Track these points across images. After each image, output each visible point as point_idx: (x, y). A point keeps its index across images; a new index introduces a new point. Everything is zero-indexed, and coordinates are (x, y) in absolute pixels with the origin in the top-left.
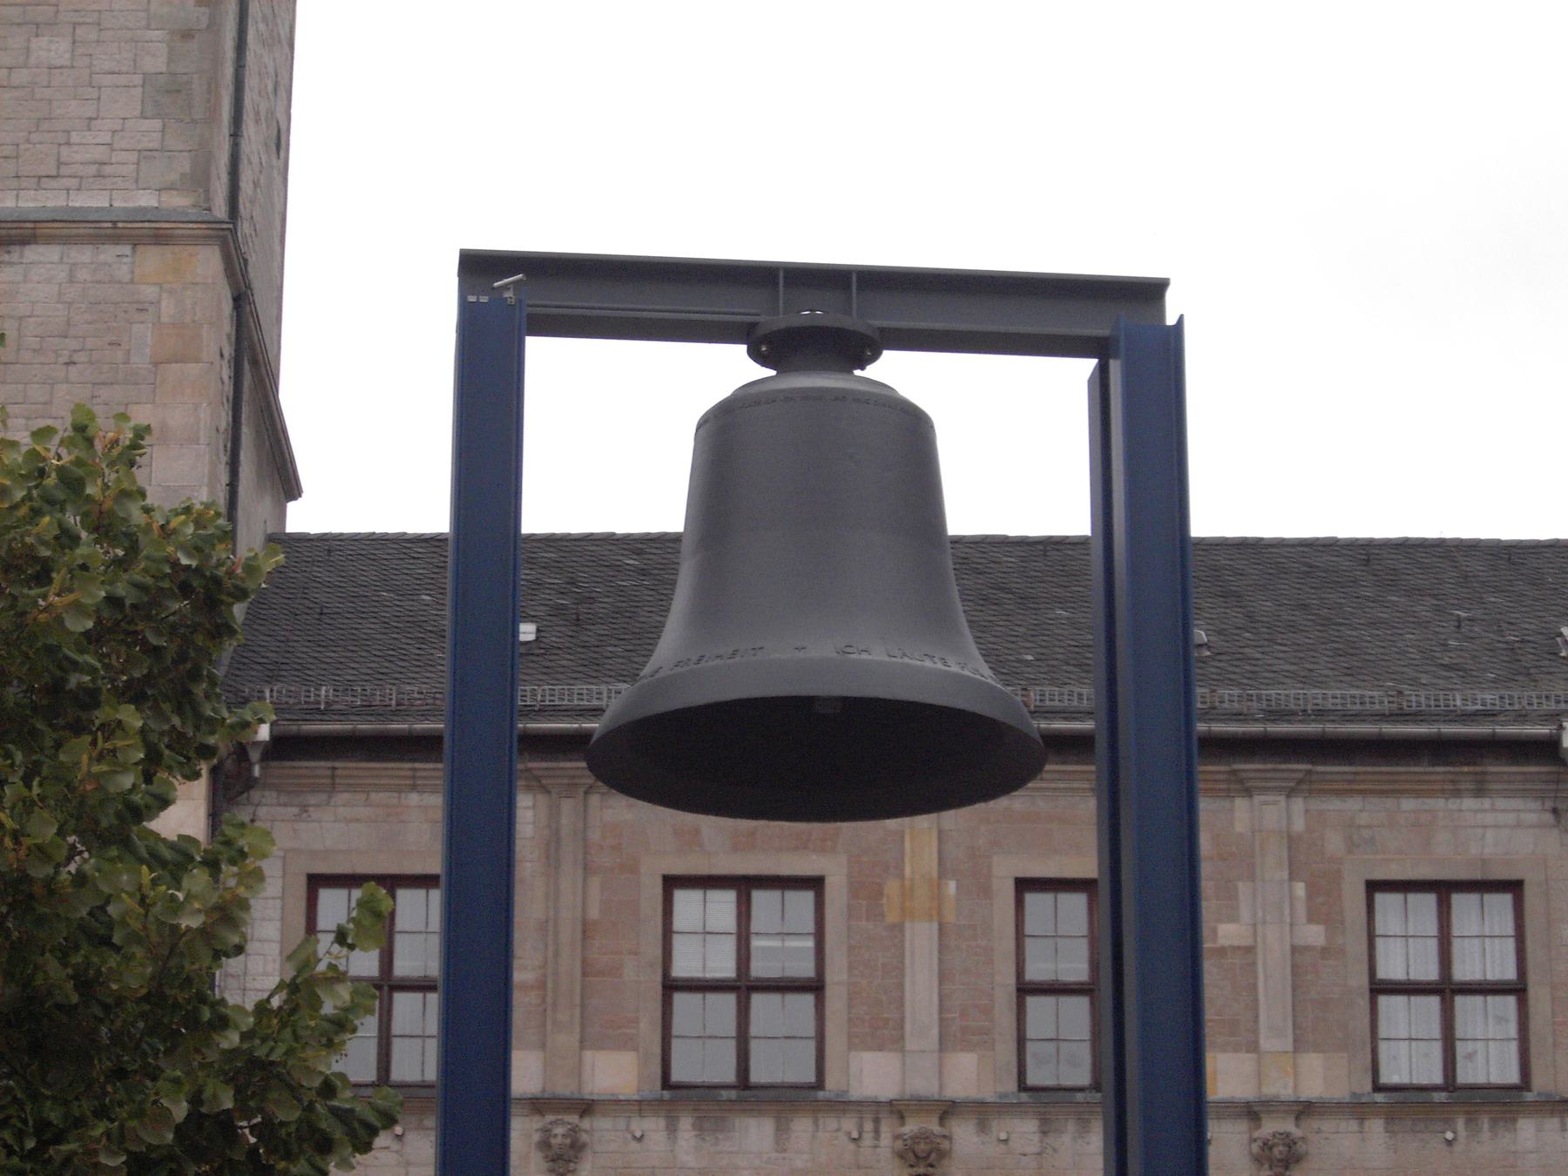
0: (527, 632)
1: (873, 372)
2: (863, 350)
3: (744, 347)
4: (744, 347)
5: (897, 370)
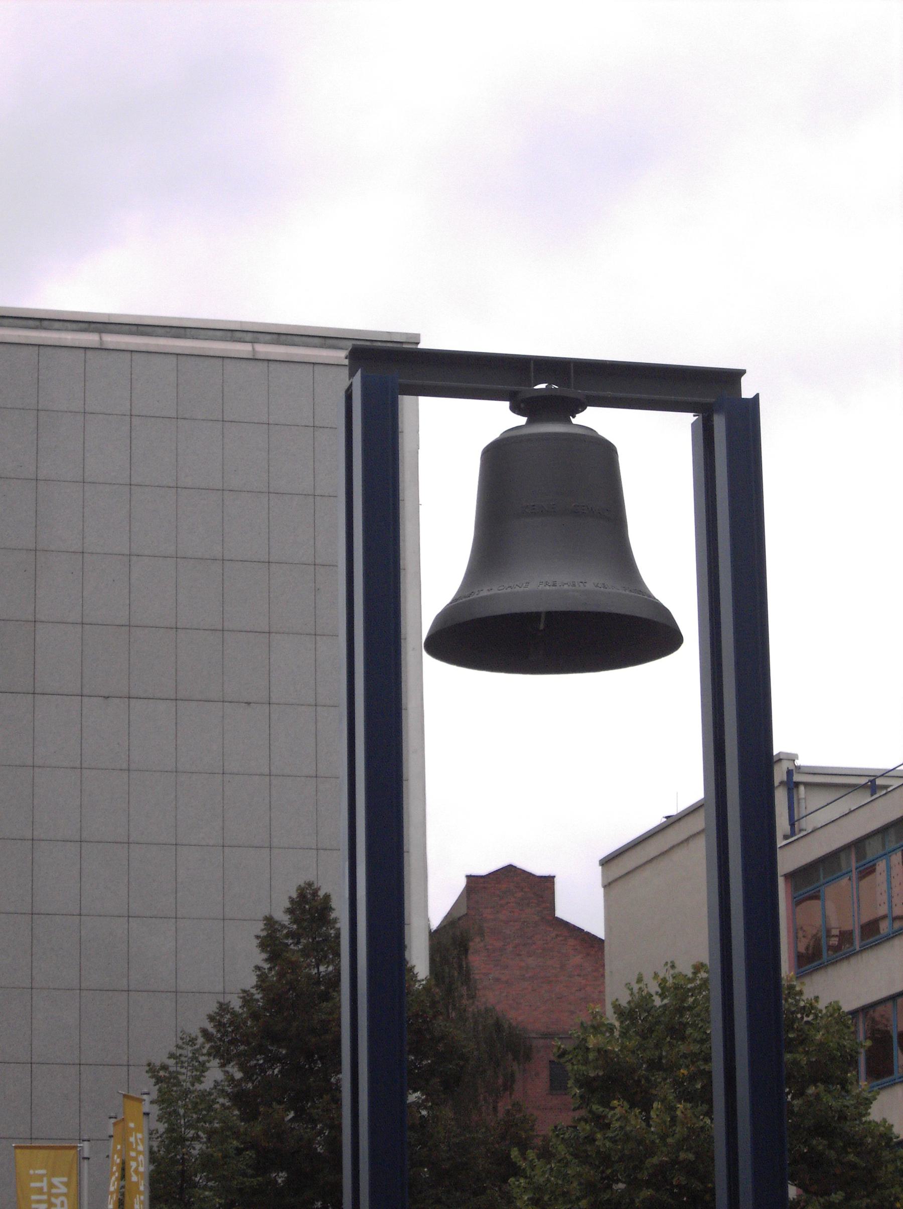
0: (793, 1192)
1: (580, 419)
2: (579, 406)
3: (507, 404)
4: (507, 404)
5: (595, 419)
